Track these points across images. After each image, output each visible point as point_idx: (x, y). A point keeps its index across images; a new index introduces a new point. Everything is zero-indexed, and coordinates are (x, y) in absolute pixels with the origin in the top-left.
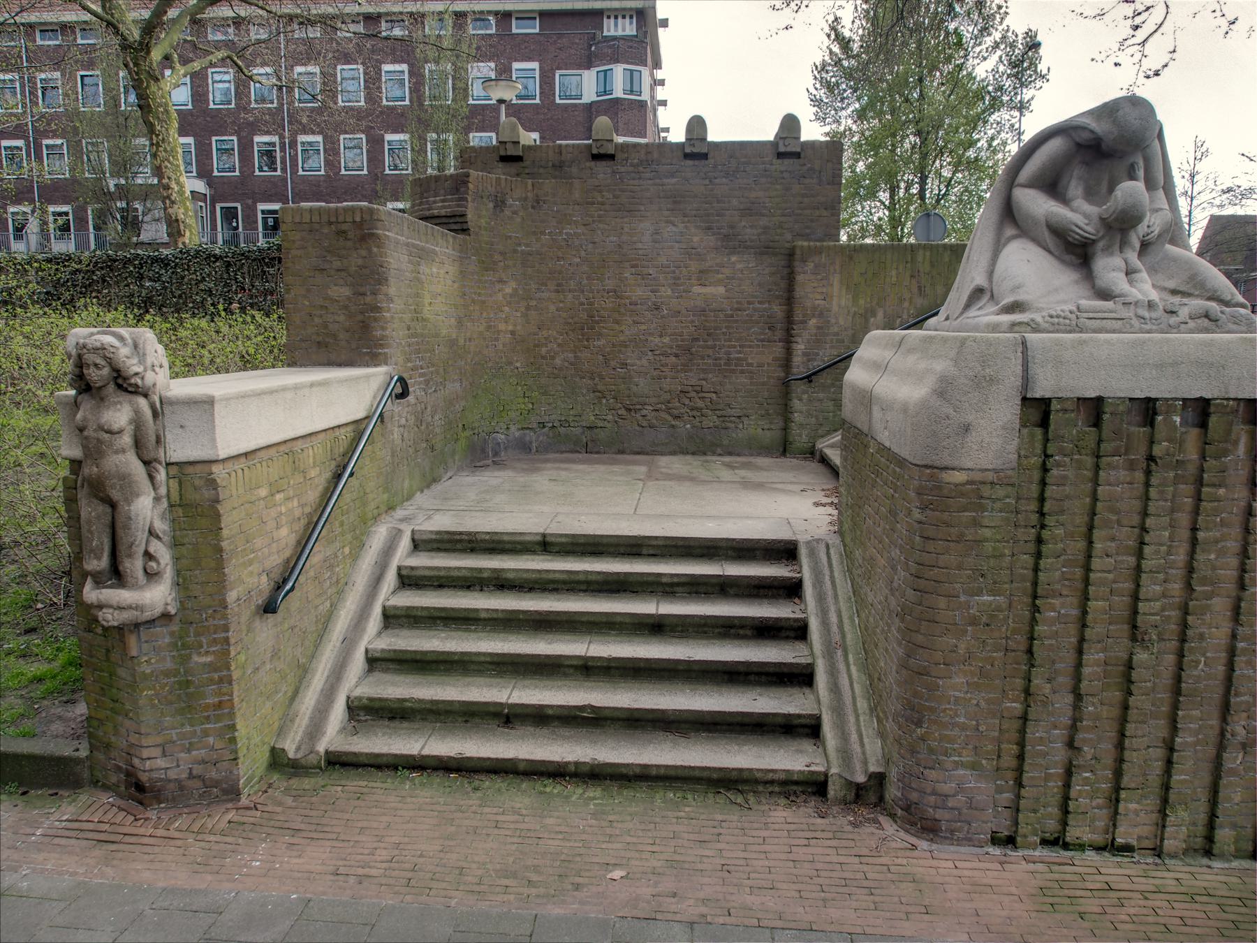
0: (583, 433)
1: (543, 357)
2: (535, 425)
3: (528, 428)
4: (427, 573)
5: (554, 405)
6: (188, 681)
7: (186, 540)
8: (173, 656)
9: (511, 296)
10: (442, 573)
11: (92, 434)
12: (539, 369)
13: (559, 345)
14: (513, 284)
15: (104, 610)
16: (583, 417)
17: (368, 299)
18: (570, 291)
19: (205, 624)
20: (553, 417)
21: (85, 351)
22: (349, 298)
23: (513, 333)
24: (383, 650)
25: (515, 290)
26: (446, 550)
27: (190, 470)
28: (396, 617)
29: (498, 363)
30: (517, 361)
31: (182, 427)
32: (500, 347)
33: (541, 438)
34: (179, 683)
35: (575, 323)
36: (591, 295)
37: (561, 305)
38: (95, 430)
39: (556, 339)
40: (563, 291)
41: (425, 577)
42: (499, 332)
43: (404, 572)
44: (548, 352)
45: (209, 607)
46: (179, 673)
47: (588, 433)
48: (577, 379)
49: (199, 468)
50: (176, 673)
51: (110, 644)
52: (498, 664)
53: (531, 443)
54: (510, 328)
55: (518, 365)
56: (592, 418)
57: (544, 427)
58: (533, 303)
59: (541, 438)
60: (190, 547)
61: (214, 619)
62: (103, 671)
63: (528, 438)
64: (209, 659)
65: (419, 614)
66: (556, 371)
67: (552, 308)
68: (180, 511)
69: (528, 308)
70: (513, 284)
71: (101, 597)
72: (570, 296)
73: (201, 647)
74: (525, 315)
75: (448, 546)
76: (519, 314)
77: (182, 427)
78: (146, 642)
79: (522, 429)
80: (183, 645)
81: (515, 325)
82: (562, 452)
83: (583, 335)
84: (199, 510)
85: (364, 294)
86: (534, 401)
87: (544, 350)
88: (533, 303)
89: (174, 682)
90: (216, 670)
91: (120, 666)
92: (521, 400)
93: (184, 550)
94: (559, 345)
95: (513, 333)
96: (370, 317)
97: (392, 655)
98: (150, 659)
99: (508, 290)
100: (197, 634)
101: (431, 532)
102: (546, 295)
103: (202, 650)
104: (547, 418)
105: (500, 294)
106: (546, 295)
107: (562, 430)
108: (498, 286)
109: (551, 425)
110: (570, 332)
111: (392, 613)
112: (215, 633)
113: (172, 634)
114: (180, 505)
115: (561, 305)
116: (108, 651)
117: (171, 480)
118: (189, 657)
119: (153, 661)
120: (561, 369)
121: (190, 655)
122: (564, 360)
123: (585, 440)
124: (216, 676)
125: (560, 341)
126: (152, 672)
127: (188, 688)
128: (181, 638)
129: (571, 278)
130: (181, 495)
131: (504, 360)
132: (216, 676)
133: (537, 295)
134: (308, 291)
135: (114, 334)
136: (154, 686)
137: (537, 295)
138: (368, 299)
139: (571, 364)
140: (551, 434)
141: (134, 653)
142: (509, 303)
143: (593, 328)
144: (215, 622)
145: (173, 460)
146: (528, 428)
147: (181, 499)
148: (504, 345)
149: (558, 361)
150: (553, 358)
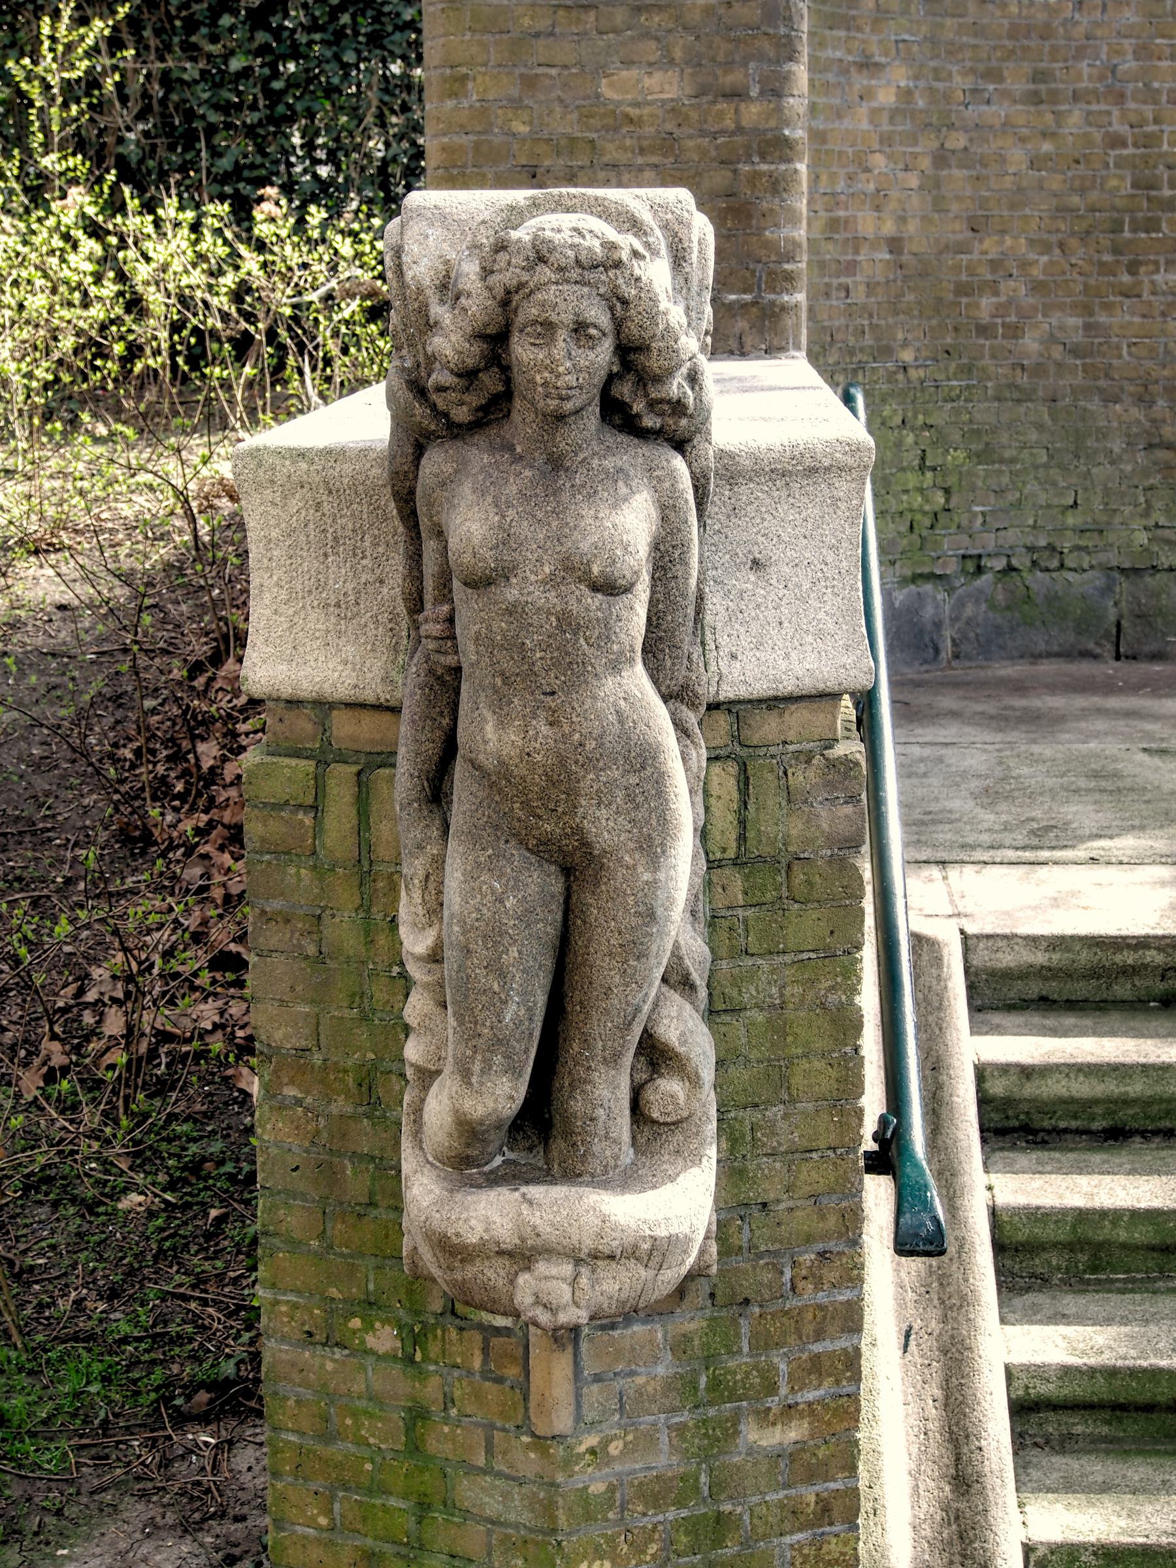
0: (1108, 589)
1: (984, 330)
2: (952, 567)
3: (931, 577)
4: (1082, 1089)
5: (1013, 496)
6: (719, 1518)
7: (749, 994)
8: (681, 1429)
9: (894, 113)
10: (1136, 1088)
11: (540, 597)
12: (967, 370)
13: (1038, 287)
14: (900, 75)
15: (541, 1267)
16: (1111, 537)
17: (753, 112)
18: (1076, 97)
19: (792, 1303)
20: (1012, 536)
21: (545, 273)
22: (674, 110)
23: (895, 245)
24: (1067, 1372)
25: (906, 94)
26: (1073, 1005)
27: (767, 728)
28: (1031, 1248)
29: (851, 352)
30: (905, 344)
31: (756, 564)
32: (859, 295)
33: (969, 610)
34: (692, 1526)
35: (1092, 209)
36: (1148, 111)
37: (1047, 147)
38: (551, 582)
39: (1024, 265)
40: (1054, 97)
41: (1071, 1101)
42: (856, 243)
43: (997, 1088)
44: (1000, 310)
45: (809, 1239)
46: (697, 1489)
47: (1123, 585)
48: (1094, 404)
49: (797, 718)
50: (689, 1482)
51: (431, 1390)
52: (1118, 1409)
53: (938, 625)
54: (889, 228)
55: (907, 356)
56: (1142, 538)
57: (979, 570)
58: (958, 140)
59: (969, 610)
60: (760, 1017)
61: (819, 1285)
62: (388, 1492)
63: (929, 612)
64: (793, 1433)
65: (1123, 1235)
66: (1023, 380)
67: (1017, 157)
68: (737, 883)
69: (941, 158)
70: (900, 75)
71: (535, 1218)
72: (1075, 118)
73: (771, 1388)
74: (932, 186)
75: (1081, 989)
76: (913, 181)
77: (756, 564)
78: (598, 1378)
79: (916, 578)
80: (715, 1384)
81: (902, 220)
82: (1036, 657)
83: (1116, 251)
84: (799, 877)
85: (737, 95)
86: (952, 480)
87: (986, 303)
88: (958, 140)
89: (677, 1525)
90: (811, 1476)
91: (473, 1471)
92: (912, 480)
93: (737, 1028)
94: (1038, 287)
95: (895, 245)
96: (756, 176)
97: (1101, 1390)
98: (606, 1442)
99: (886, 97)
100: (763, 1343)
101: (1033, 941)
102: (997, 112)
103: (773, 1403)
104: (990, 541)
105: (863, 110)
106: (997, 112)
107: (1038, 581)
108: (860, 81)
109: (999, 564)
110: (1074, 242)
111: (1021, 1236)
112: (819, 1336)
113: (680, 1346)
114: (736, 863)
115: (1047, 147)
116: (418, 1415)
117: (717, 768)
118: (730, 1429)
119: (615, 1448)
120: (1038, 370)
121: (736, 1418)
122: (1052, 339)
123: (1112, 614)
124: (809, 1494)
125: (1036, 272)
126: (612, 1489)
127: (718, 1543)
128: (709, 1360)
129: (1080, 53)
130: (743, 823)
131: (868, 340)
132: (809, 1494)
133: (973, 113)
134: (530, 83)
135: (604, 212)
136: (611, 1541)
137: (973, 113)
138: (753, 112)
139: (1075, 351)
140: (1000, 597)
141: (563, 1421)
142: (887, 140)
143: (1152, 225)
144: (822, 1297)
145: (728, 692)
146: (931, 577)
147: (742, 838)
148: (871, 287)
149: (1030, 343)
150: (1014, 332)
